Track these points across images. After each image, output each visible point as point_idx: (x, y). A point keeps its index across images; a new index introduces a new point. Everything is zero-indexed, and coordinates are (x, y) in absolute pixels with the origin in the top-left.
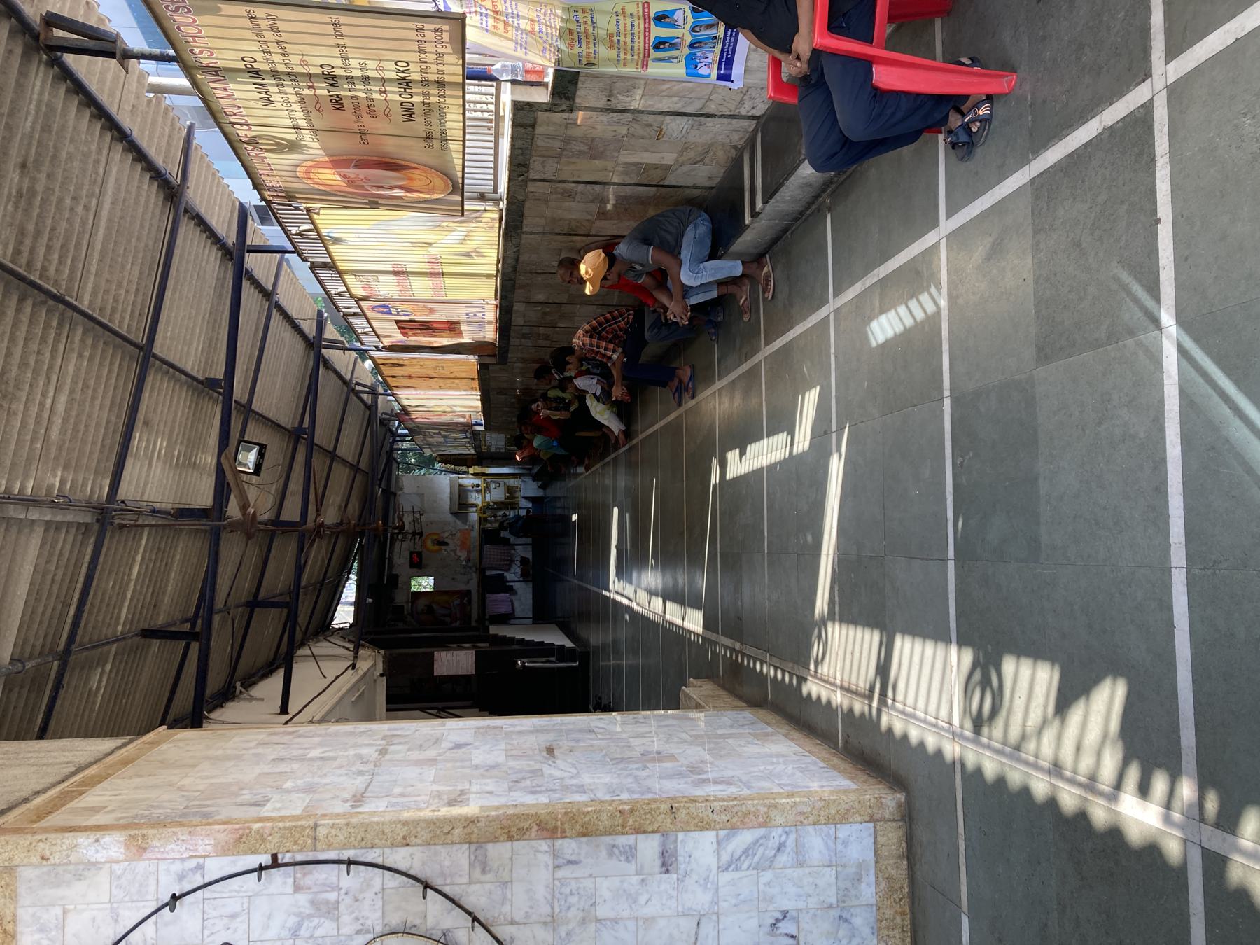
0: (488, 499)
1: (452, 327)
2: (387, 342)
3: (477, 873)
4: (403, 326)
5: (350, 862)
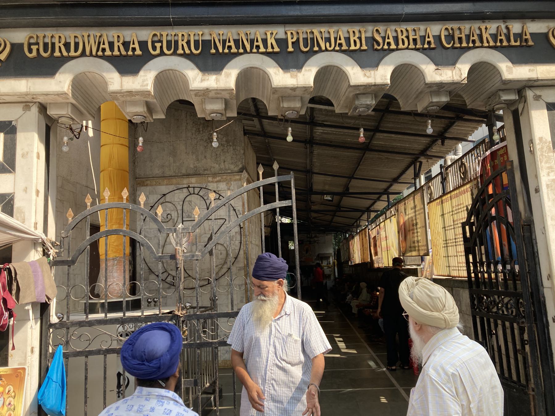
0: (325, 268)
1: (376, 254)
2: (370, 232)
3: (238, 268)
4: (375, 237)
5: (241, 242)
